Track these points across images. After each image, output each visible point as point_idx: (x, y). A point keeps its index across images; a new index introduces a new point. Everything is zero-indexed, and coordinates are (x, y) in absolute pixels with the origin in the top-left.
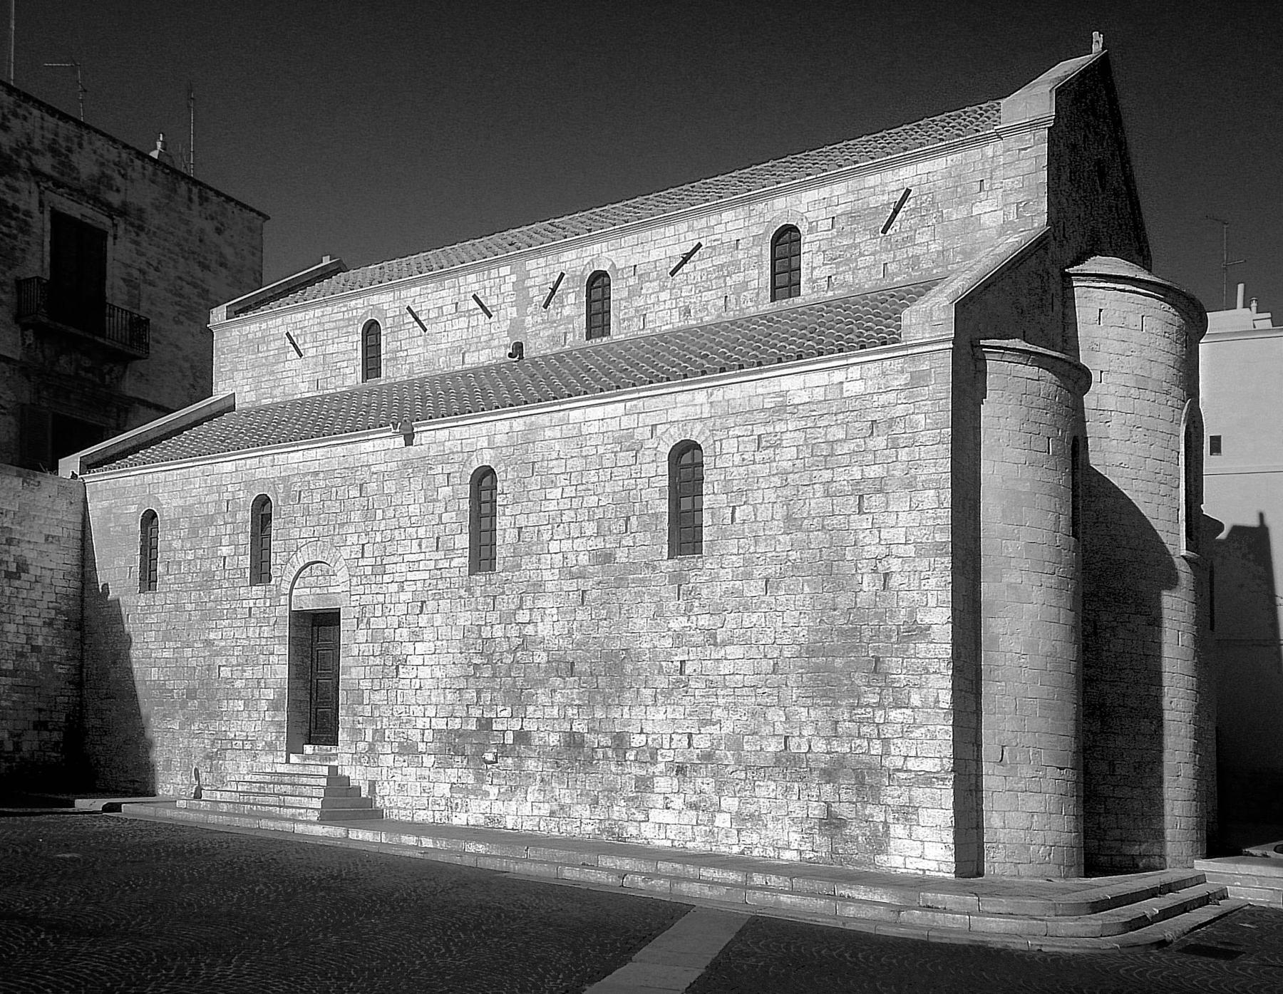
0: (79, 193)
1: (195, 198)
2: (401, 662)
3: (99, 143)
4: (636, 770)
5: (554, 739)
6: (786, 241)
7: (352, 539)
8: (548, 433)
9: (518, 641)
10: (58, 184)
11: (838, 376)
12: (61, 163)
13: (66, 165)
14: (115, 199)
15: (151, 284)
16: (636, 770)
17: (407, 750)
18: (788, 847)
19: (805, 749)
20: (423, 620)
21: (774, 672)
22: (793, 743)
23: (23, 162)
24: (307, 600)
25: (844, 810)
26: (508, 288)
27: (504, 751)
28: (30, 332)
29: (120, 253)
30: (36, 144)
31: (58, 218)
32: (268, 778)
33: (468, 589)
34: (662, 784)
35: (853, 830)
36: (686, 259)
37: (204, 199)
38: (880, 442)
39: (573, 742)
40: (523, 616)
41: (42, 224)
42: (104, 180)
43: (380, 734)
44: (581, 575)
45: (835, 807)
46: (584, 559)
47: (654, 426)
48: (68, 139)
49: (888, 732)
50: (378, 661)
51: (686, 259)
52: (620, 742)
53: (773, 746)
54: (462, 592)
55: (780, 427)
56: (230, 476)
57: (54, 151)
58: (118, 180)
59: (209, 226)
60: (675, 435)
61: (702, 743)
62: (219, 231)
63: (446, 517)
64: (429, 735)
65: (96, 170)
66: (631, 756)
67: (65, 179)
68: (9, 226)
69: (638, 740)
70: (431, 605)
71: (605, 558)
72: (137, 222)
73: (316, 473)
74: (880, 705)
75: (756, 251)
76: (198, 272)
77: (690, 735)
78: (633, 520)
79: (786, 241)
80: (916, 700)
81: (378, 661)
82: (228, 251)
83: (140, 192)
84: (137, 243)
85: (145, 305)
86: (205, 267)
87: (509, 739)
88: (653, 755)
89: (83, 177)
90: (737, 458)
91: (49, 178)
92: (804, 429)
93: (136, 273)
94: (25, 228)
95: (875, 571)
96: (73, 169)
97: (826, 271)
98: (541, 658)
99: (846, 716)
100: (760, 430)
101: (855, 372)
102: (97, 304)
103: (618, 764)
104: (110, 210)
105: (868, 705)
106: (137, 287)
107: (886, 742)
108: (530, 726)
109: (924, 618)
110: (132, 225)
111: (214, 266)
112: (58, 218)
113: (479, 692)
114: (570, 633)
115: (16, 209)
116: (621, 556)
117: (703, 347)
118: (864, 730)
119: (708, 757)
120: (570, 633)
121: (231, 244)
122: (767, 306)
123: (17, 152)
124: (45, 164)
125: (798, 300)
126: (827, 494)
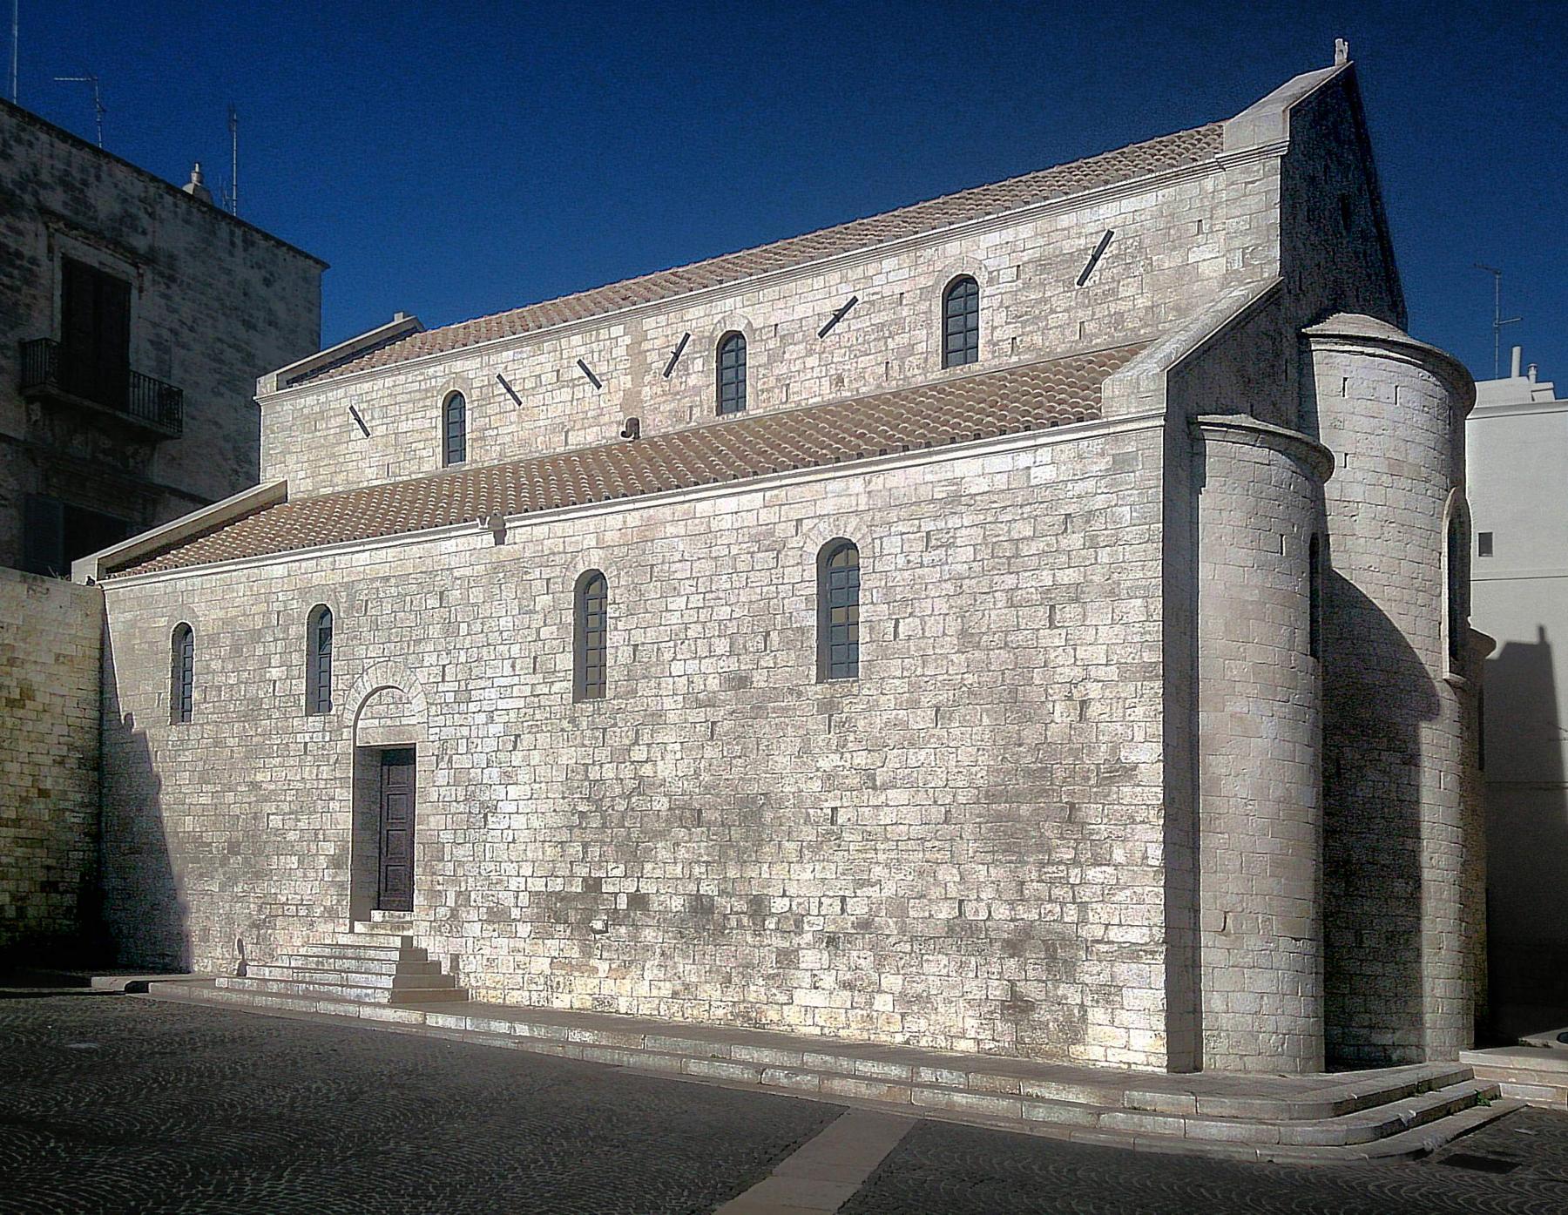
1: (239, 242)
2: (490, 809)
4: (778, 942)
5: (677, 904)
6: (960, 294)
7: (430, 659)
8: (670, 530)
9: (633, 784)
10: (71, 225)
11: (1025, 460)
12: (75, 199)
13: (80, 201)
14: (140, 243)
15: (184, 346)
16: (778, 942)
17: (497, 916)
18: (963, 1035)
19: (983, 915)
20: (517, 758)
21: (946, 822)
22: (969, 908)
23: (28, 198)
24: (376, 734)
25: (1032, 991)
26: (620, 352)
27: (615, 917)
28: (36, 406)
29: (147, 309)
30: (45, 177)
31: (71, 267)
32: (327, 951)
33: (573, 721)
34: (809, 958)
35: (1042, 1014)
38: (1075, 540)
39: (701, 907)
40: (639, 754)
41: (51, 274)
43: (464, 898)
44: (710, 703)
45: (1021, 987)
46: (713, 683)
48: (83, 170)
49: (1086, 894)
50: (462, 807)
52: (758, 907)
53: (945, 912)
54: (565, 724)
55: (954, 522)
57: (65, 182)
58: (145, 221)
59: (256, 277)
61: (858, 908)
62: (267, 282)
63: (545, 633)
64: (524, 899)
65: (117, 208)
66: (771, 924)
67: (80, 219)
68: (11, 276)
69: (780, 905)
70: (527, 740)
71: (740, 682)
72: (167, 272)
73: (386, 579)
74: (1075, 862)
75: (924, 306)
76: (241, 332)
78: (774, 635)
79: (960, 294)
80: (1119, 855)
81: (462, 807)
82: (279, 308)
83: (171, 234)
85: (177, 372)
86: (250, 326)
87: (623, 903)
88: (799, 923)
89: (102, 216)
90: (901, 561)
91: (60, 217)
92: (982, 525)
93: (165, 334)
94: (30, 279)
95: (1070, 698)
96: (89, 207)
98: (661, 804)
99: (1034, 875)
100: (929, 525)
101: (1045, 455)
103: (756, 934)
105: (1060, 862)
106: (167, 351)
107: (1083, 907)
108: (647, 888)
109: (1129, 755)
110: (161, 274)
111: (261, 325)
112: (71, 267)
113: (585, 846)
114: (697, 774)
115: (19, 255)
116: (759, 679)
117: (859, 424)
118: (1056, 892)
119: (865, 925)
120: (697, 774)
122: (937, 374)
124: (56, 200)
125: (976, 367)
126: (1011, 604)
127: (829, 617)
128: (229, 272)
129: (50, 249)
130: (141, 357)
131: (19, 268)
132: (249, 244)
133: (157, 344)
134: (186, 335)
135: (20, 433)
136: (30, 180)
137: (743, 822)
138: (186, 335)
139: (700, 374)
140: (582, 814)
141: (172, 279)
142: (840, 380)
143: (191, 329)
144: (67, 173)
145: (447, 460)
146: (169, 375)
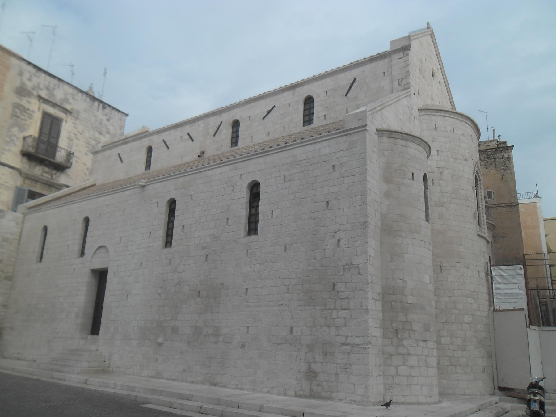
0: (54, 105)
3: (66, 87)
13: (52, 94)
14: (68, 107)
15: (78, 139)
23: (35, 93)
24: (98, 266)
25: (316, 367)
29: (67, 128)
30: (41, 86)
31: (46, 115)
36: (269, 112)
37: (104, 108)
41: (38, 117)
42: (66, 100)
47: (241, 175)
51: (269, 112)
56: (76, 211)
57: (48, 88)
58: (71, 100)
59: (105, 118)
60: (248, 180)
62: (108, 120)
66: (221, 339)
68: (24, 116)
72: (76, 116)
73: (108, 206)
74: (335, 309)
76: (97, 135)
77: (248, 327)
78: (230, 219)
83: (79, 104)
84: (74, 124)
86: (100, 133)
93: (72, 135)
94: (31, 117)
97: (324, 113)
102: (53, 147)
104: (66, 111)
105: (329, 309)
106: (72, 140)
110: (74, 117)
111: (104, 133)
112: (46, 115)
115: (28, 110)
121: (112, 125)
123: (33, 89)
124: (44, 94)
125: (312, 126)
127: (256, 212)
128: (96, 116)
129: (39, 109)
130: (63, 142)
131: (28, 114)
132: (104, 108)
133: (70, 139)
134: (79, 136)
135: (18, 165)
136: (37, 87)
137: (211, 295)
138: (79, 136)
139: (226, 133)
140: (159, 294)
141: (77, 118)
142: (269, 134)
143: (81, 134)
144: (49, 86)
145: (146, 169)
146: (71, 148)
